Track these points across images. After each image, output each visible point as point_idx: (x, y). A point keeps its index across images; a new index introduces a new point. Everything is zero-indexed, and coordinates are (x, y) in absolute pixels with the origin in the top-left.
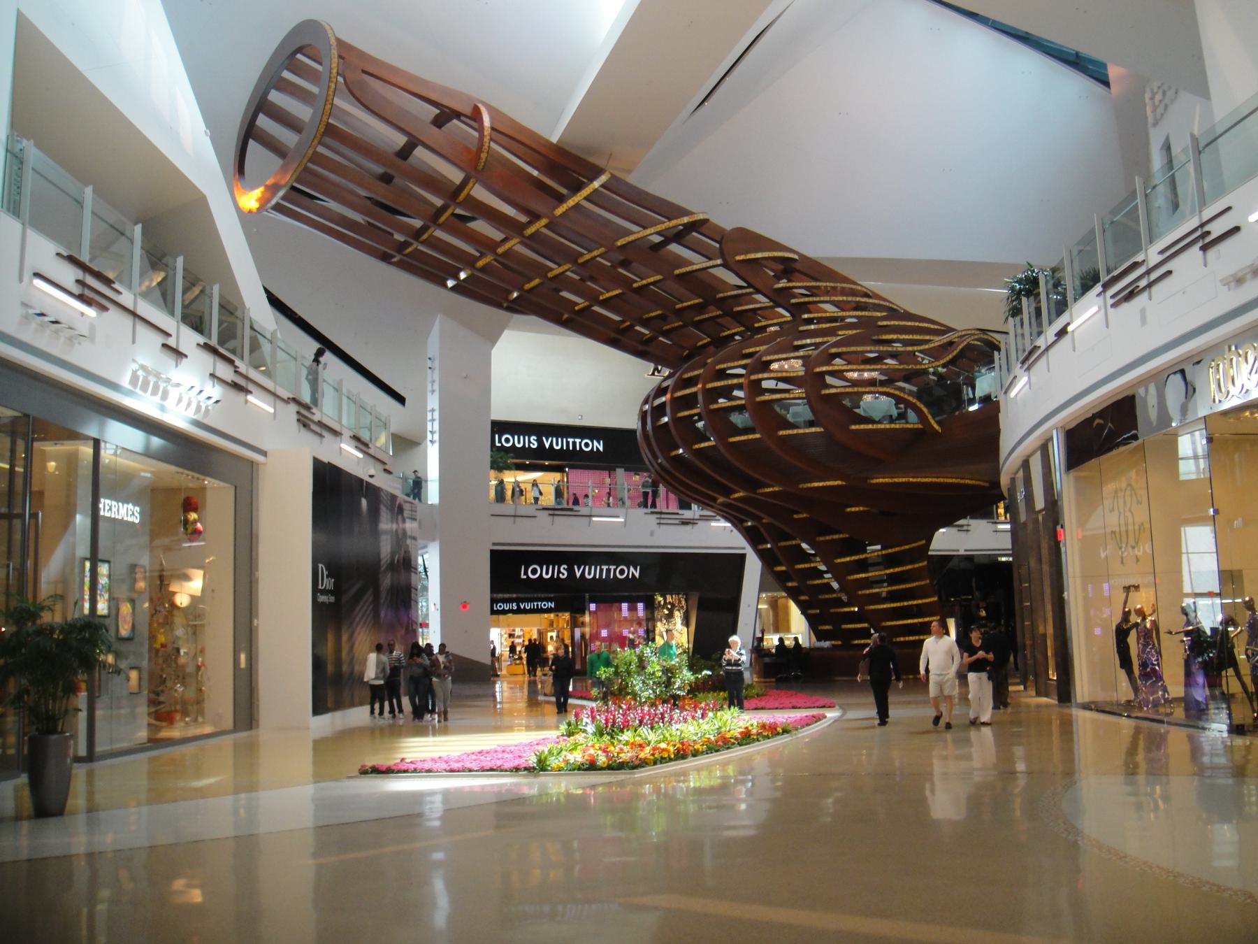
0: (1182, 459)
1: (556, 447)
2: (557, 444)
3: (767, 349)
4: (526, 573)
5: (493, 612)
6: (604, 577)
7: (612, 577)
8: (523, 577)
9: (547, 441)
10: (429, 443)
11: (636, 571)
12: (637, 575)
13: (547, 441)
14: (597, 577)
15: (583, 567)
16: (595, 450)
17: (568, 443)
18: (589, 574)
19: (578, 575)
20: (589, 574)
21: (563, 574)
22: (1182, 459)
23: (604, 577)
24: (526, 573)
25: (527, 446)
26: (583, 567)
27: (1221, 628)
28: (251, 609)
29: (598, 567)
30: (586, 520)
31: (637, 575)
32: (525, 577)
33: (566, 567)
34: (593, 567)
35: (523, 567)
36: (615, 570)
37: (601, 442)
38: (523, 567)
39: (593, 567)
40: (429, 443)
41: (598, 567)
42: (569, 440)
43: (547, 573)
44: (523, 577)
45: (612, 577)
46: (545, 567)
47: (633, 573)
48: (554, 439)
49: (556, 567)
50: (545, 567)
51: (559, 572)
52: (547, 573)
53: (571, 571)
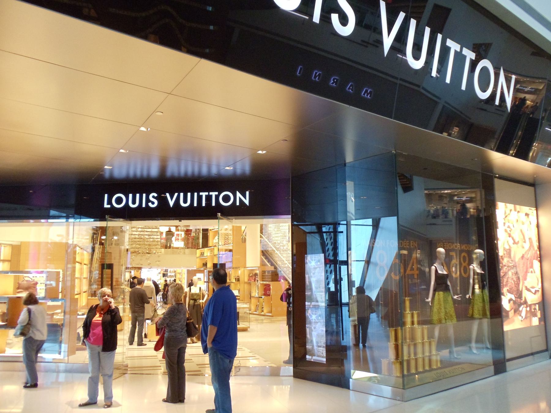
1: (183, 205)
2: (185, 201)
3: (506, 107)
4: (110, 202)
5: (109, 405)
6: (204, 205)
7: (214, 204)
8: (106, 206)
9: (172, 198)
11: (245, 197)
12: (247, 202)
13: (172, 198)
14: (195, 205)
15: (176, 194)
16: (238, 204)
17: (200, 198)
18: (185, 202)
19: (171, 203)
20: (185, 202)
21: (153, 203)
23: (204, 205)
24: (110, 202)
25: (144, 206)
26: (176, 194)
29: (196, 194)
31: (247, 202)
32: (109, 206)
33: (156, 195)
35: (106, 196)
36: (217, 197)
37: (247, 193)
38: (106, 196)
41: (196, 194)
42: (201, 194)
43: (134, 202)
44: (106, 206)
45: (214, 204)
46: (131, 196)
47: (240, 199)
48: (182, 195)
49: (144, 195)
50: (131, 196)
51: (148, 200)
52: (134, 202)
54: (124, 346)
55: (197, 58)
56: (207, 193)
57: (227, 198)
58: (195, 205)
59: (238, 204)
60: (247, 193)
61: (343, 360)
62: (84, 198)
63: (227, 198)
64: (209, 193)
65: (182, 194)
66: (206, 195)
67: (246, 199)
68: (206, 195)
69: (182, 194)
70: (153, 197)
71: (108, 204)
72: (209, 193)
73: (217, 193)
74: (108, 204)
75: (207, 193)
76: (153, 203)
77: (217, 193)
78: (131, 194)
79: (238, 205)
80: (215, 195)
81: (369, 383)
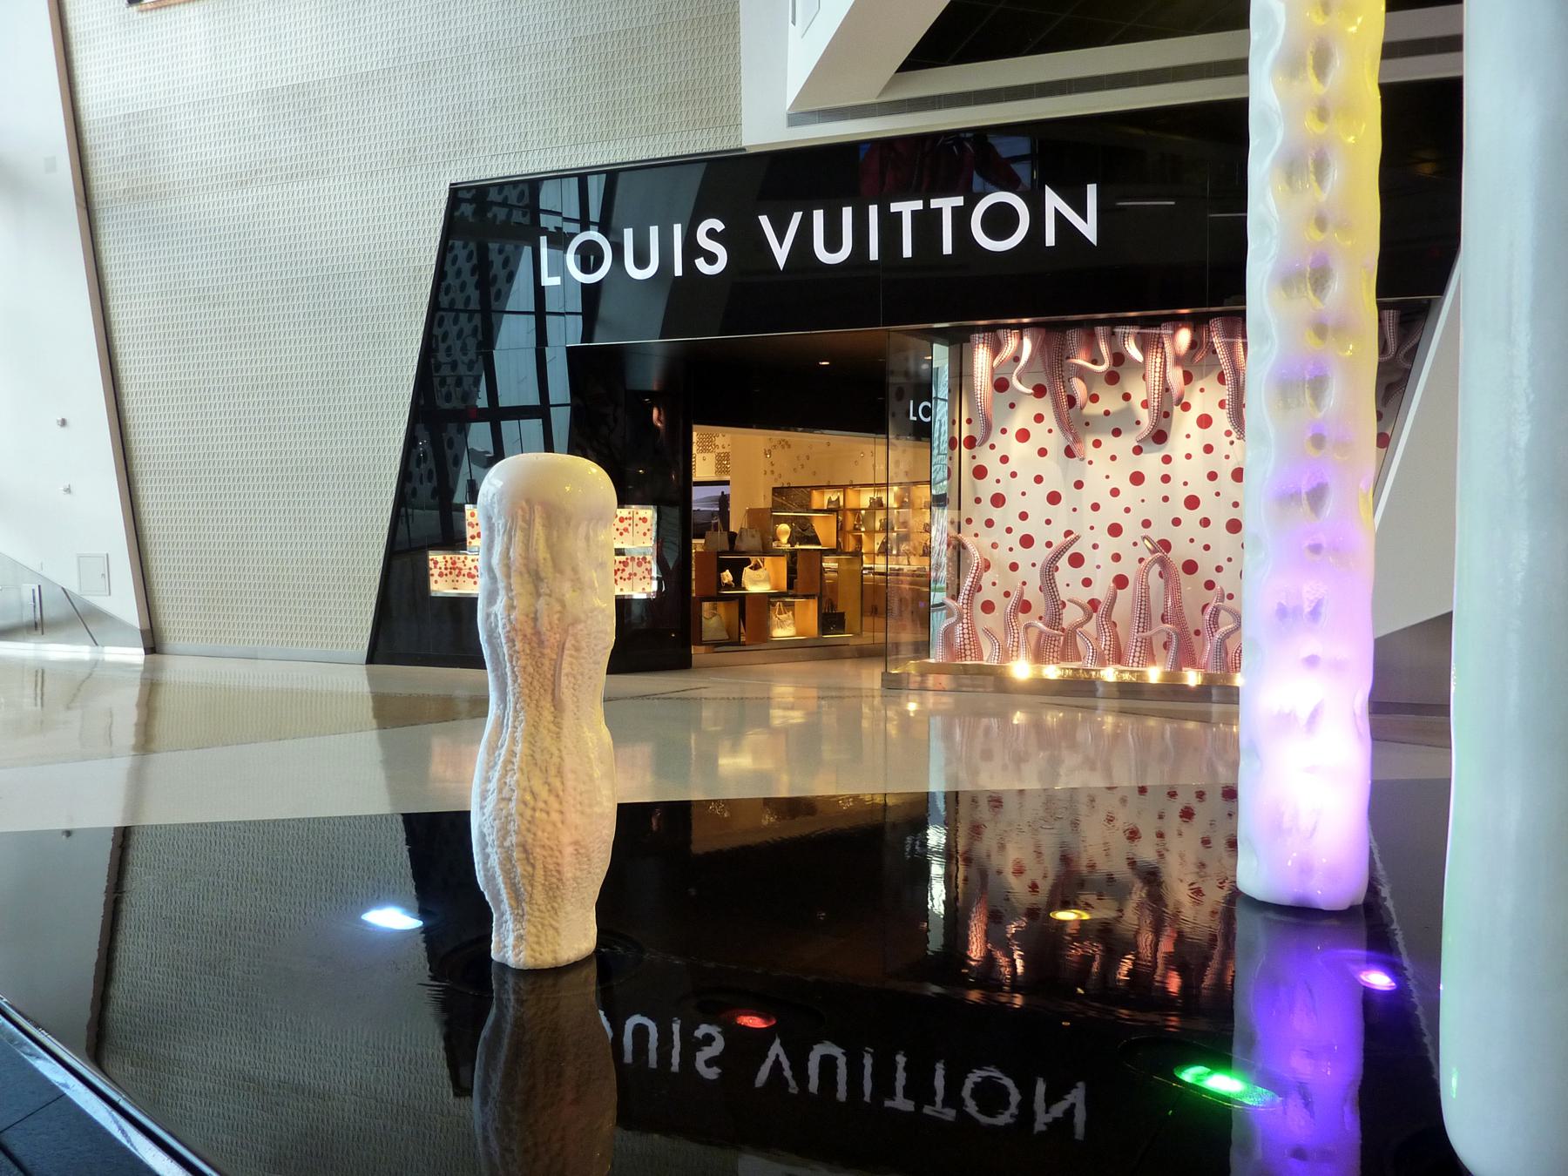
0: (494, 311)
6: (874, 254)
10: (1231, 428)
12: (1089, 228)
15: (797, 217)
16: (1050, 240)
17: (891, 225)
18: (833, 244)
19: (781, 254)
20: (833, 244)
21: (711, 258)
22: (494, 311)
26: (797, 217)
27: (1063, 744)
28: (79, 570)
29: (873, 210)
30: (919, 511)
31: (1089, 228)
32: (915, 419)
33: (719, 226)
34: (847, 213)
36: (961, 218)
37: (1092, 190)
39: (847, 213)
40: (1231, 428)
41: (873, 210)
53: (745, 243)
54: (552, 912)
55: (122, 618)
56: (918, 205)
57: (1000, 222)
58: (874, 254)
59: (1050, 240)
60: (1092, 190)
61: (749, 524)
62: (827, 363)
63: (1000, 222)
64: (927, 204)
65: (818, 216)
66: (914, 212)
67: (1085, 219)
68: (914, 212)
69: (818, 216)
70: (711, 234)
71: (914, 416)
72: (927, 204)
73: (959, 201)
74: (914, 416)
75: (918, 205)
76: (711, 258)
77: (959, 201)
78: (680, 225)
79: (675, 226)
80: (912, 211)
81: (1294, 1164)
